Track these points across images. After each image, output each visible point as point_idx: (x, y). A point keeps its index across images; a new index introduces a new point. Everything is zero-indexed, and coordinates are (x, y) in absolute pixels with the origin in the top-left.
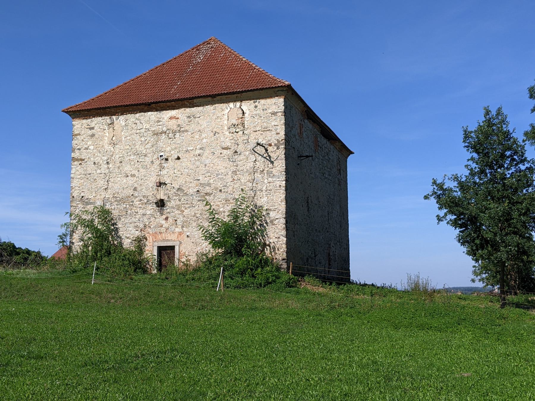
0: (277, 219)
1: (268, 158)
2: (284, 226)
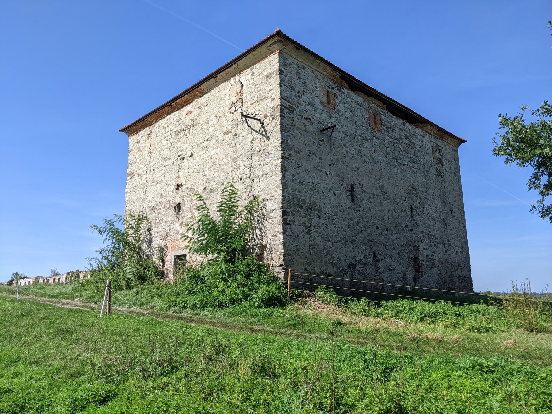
0: (273, 210)
1: (264, 133)
2: (281, 219)
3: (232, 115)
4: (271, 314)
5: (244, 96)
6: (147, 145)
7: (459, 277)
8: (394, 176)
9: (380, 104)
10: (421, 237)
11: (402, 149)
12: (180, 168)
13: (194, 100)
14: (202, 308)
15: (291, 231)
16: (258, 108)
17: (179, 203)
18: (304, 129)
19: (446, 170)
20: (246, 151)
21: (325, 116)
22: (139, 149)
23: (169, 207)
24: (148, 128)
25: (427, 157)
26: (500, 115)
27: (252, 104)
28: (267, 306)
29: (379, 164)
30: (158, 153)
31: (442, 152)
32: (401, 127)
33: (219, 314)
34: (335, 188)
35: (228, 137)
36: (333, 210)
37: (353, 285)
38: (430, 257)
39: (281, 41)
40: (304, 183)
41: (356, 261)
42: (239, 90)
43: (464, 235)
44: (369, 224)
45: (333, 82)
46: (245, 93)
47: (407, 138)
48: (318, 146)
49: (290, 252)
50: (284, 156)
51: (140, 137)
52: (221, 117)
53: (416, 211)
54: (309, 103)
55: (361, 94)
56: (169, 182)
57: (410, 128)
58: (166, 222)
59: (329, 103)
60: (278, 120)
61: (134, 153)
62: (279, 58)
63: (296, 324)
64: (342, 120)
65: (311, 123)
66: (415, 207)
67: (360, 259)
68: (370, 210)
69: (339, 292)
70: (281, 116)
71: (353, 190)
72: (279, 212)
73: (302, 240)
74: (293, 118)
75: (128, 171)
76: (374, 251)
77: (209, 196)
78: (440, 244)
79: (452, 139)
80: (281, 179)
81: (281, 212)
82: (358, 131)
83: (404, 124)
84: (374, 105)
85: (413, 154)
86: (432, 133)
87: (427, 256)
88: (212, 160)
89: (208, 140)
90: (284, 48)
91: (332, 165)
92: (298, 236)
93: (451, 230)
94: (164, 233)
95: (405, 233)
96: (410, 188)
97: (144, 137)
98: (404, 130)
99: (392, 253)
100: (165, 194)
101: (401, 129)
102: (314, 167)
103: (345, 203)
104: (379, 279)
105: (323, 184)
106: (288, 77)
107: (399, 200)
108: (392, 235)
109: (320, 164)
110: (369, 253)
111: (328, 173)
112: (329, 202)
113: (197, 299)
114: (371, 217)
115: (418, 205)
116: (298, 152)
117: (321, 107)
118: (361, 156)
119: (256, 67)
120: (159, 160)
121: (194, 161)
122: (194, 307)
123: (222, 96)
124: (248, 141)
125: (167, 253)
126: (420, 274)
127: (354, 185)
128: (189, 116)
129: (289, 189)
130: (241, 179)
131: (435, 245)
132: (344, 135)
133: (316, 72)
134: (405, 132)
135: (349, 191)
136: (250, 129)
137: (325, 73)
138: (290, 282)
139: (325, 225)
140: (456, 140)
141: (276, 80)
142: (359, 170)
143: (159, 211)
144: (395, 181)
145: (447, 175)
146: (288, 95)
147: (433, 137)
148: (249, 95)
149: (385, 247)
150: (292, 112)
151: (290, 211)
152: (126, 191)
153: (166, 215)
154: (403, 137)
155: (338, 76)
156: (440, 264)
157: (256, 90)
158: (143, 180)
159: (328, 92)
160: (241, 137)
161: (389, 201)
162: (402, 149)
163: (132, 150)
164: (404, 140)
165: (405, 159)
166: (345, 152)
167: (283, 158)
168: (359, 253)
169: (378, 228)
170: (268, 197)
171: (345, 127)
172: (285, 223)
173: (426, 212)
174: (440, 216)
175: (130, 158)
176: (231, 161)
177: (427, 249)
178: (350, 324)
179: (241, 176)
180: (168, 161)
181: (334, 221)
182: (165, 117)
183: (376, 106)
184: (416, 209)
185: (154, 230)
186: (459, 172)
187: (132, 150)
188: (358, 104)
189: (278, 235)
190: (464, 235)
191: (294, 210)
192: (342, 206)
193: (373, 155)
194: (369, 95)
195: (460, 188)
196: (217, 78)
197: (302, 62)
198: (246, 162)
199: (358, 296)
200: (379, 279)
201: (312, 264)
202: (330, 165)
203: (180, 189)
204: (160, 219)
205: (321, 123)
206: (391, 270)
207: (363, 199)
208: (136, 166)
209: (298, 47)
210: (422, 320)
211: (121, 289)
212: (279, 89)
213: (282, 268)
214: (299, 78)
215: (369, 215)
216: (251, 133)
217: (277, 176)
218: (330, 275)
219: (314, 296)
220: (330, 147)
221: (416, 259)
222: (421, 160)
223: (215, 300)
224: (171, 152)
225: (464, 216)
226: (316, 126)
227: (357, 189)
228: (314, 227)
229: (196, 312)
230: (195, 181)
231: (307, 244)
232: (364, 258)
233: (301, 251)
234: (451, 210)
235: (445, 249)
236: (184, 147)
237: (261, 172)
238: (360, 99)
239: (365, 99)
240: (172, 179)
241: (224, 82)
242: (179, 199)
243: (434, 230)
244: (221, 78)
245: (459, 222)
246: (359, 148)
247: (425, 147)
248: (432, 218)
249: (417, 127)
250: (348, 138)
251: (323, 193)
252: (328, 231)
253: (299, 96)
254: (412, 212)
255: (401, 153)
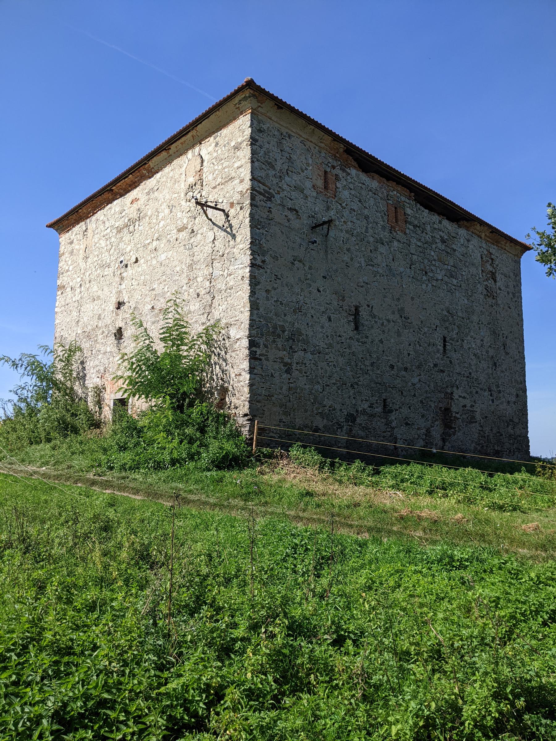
0: (238, 339)
1: (229, 230)
2: (247, 352)
3: (188, 203)
4: (221, 480)
5: (204, 176)
6: (82, 246)
7: (510, 436)
8: (421, 296)
9: (406, 191)
10: (456, 381)
11: (435, 257)
12: (122, 279)
13: (142, 182)
14: (133, 470)
15: (262, 368)
16: (222, 194)
17: (121, 328)
18: (287, 224)
19: (500, 289)
20: (205, 255)
21: (319, 207)
22: (72, 253)
23: (108, 333)
24: (83, 223)
25: (473, 270)
26: (549, 205)
27: (214, 188)
28: (219, 468)
29: (399, 278)
30: (96, 259)
31: (497, 263)
32: (435, 226)
33: (153, 478)
34: (330, 310)
35: (183, 235)
36: (326, 341)
37: (349, 445)
38: (468, 408)
39: (254, 96)
40: (284, 302)
41: (357, 411)
42: (198, 168)
43: (522, 379)
44: (380, 362)
45: (335, 158)
46: (206, 171)
47: (443, 241)
48: (308, 250)
49: (260, 398)
50: (254, 262)
51: (74, 235)
52: (175, 207)
53: (452, 344)
54: (295, 187)
55: (376, 176)
56: (108, 298)
57: (450, 228)
58: (104, 353)
59: (326, 188)
60: (247, 212)
61: (66, 257)
62: (251, 120)
63: (249, 493)
64: (346, 213)
65: (298, 217)
66: (451, 339)
67: (364, 409)
68: (381, 341)
69: (324, 453)
70: (251, 205)
71: (358, 314)
72: (245, 343)
73: (278, 381)
74: (270, 208)
75: (59, 282)
76: (384, 398)
77: (157, 319)
78: (485, 390)
79: (512, 244)
80: (250, 296)
81: (248, 342)
82: (369, 229)
83: (440, 222)
84: (395, 193)
85: (452, 264)
86: (483, 236)
87: (465, 406)
88: (162, 268)
89: (157, 239)
90: (260, 106)
91: (328, 277)
92: (272, 375)
93: (502, 372)
94: (102, 369)
95: (432, 374)
96: (445, 313)
97: (78, 236)
98: (440, 230)
99: (411, 401)
100: (103, 315)
101: (435, 229)
102: (300, 279)
103: (345, 332)
104: (390, 437)
105: (313, 304)
106: (264, 149)
107: (426, 329)
108: (413, 377)
109: (309, 276)
110: (377, 400)
111: (321, 289)
112: (321, 330)
113: (127, 457)
114: (383, 351)
115: (455, 336)
116: (276, 258)
117: (315, 194)
118: (373, 266)
119: (220, 134)
120: (97, 267)
121: (140, 269)
122: (123, 468)
123: (177, 176)
124: (208, 241)
125: (106, 396)
126: (453, 430)
127: (359, 307)
128: (135, 205)
129: (261, 310)
130: (198, 295)
131: (477, 392)
132: (347, 235)
133: (308, 143)
134: (441, 233)
135: (352, 315)
136: (211, 223)
137: (323, 145)
138: (256, 437)
139: (313, 362)
140: (517, 247)
141: (246, 153)
142: (369, 286)
143: (96, 339)
144: (423, 302)
145: (502, 295)
146: (263, 174)
147: (484, 242)
148: (212, 174)
149: (402, 393)
150: (269, 199)
151: (261, 341)
152: (56, 310)
153: (104, 344)
154: (438, 241)
155: (341, 150)
156: (483, 418)
157: (220, 167)
158: (77, 295)
159: (326, 172)
160: (199, 235)
161: (411, 330)
162: (435, 257)
163: (63, 253)
164: (439, 245)
165: (438, 271)
166: (349, 260)
167: (252, 265)
168: (362, 401)
169: (392, 367)
170: (232, 321)
171: (349, 223)
172: (253, 357)
173: (466, 346)
174: (487, 352)
175: (60, 265)
176: (186, 269)
177: (464, 398)
178: (324, 495)
179: (198, 291)
180: (107, 269)
181: (327, 357)
182: (104, 207)
183: (398, 194)
184: (451, 341)
185: (89, 365)
186: (520, 292)
187: (63, 253)
188: (371, 191)
189: (243, 373)
190: (522, 379)
191: (267, 340)
192: (340, 336)
193: (390, 265)
194: (388, 179)
195: (520, 315)
196: (170, 151)
197: (286, 127)
198: (205, 271)
199: (349, 459)
200: (390, 437)
201: (292, 415)
202: (324, 277)
203: (122, 308)
204: (96, 349)
205: (313, 217)
206: (409, 424)
207: (372, 327)
208: (69, 276)
209: (280, 105)
210: (431, 493)
211: (38, 443)
212: (249, 165)
213: (246, 418)
214: (281, 151)
215: (381, 349)
216: (213, 229)
217: (244, 291)
218: (317, 430)
219: (288, 457)
220: (326, 251)
221: (447, 410)
222: (464, 273)
223: (150, 459)
224: (112, 257)
225: (523, 353)
226: (306, 221)
227: (364, 313)
228: (297, 364)
229: (124, 474)
230: (140, 298)
231: (285, 387)
232: (370, 407)
233: (276, 396)
234: (504, 345)
235: (491, 398)
236: (128, 250)
237: (224, 285)
238: (374, 184)
239: (382, 184)
240: (111, 295)
241: (179, 157)
242: (120, 322)
243: (477, 371)
244: (175, 150)
245: (515, 361)
246: (370, 254)
247: (471, 256)
248: (475, 355)
249: (460, 227)
250: (354, 239)
251: (312, 317)
252: (318, 370)
253: (280, 177)
254: (445, 346)
255: (433, 262)
